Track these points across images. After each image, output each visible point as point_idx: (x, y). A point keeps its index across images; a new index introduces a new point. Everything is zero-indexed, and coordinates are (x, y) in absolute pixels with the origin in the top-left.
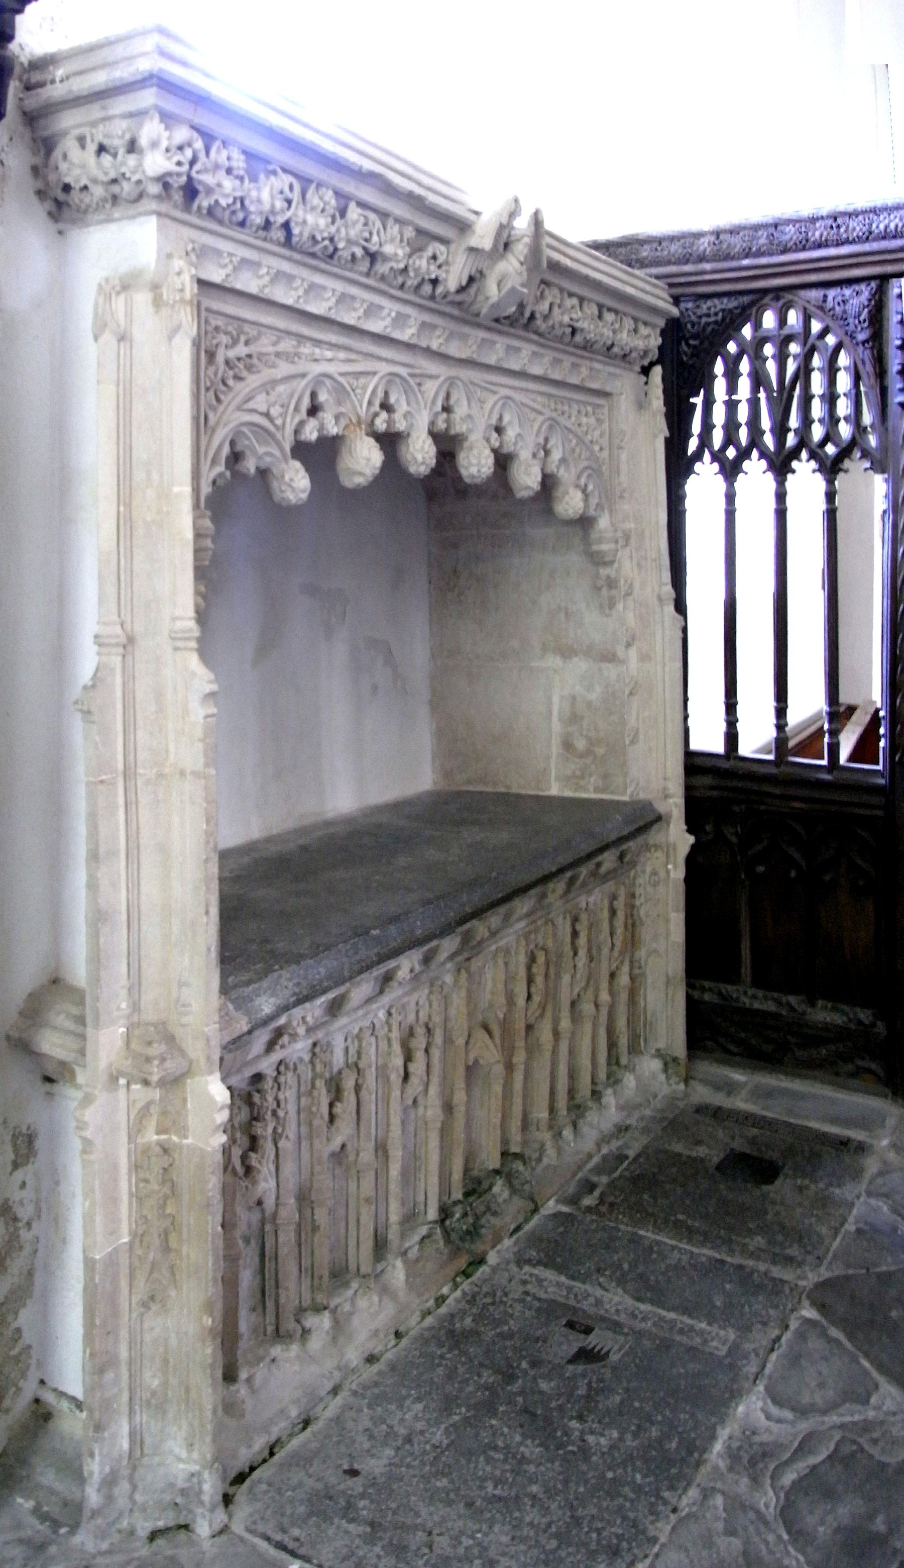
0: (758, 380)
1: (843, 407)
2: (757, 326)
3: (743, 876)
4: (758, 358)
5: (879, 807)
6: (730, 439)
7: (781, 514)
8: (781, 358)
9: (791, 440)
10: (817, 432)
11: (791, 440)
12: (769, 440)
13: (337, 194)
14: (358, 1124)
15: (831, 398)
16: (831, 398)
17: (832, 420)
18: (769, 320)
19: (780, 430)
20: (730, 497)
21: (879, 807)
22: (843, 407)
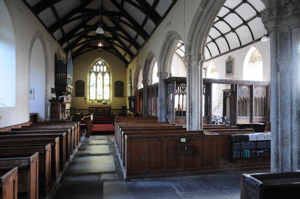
0: (181, 88)
1: (180, 91)
2: (181, 85)
3: (186, 148)
4: (181, 87)
5: (96, 68)
6: (179, 93)
7: (183, 98)
8: (183, 87)
9: (184, 93)
10: (178, 92)
11: (184, 93)
12: (182, 93)
13: (169, 123)
14: (185, 30)
15: (179, 90)
16: (179, 90)
17: (179, 91)
18: (182, 84)
19: (183, 92)
20: (179, 97)
21: (96, 68)
22: (180, 91)
